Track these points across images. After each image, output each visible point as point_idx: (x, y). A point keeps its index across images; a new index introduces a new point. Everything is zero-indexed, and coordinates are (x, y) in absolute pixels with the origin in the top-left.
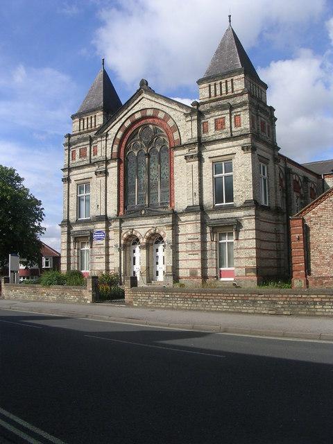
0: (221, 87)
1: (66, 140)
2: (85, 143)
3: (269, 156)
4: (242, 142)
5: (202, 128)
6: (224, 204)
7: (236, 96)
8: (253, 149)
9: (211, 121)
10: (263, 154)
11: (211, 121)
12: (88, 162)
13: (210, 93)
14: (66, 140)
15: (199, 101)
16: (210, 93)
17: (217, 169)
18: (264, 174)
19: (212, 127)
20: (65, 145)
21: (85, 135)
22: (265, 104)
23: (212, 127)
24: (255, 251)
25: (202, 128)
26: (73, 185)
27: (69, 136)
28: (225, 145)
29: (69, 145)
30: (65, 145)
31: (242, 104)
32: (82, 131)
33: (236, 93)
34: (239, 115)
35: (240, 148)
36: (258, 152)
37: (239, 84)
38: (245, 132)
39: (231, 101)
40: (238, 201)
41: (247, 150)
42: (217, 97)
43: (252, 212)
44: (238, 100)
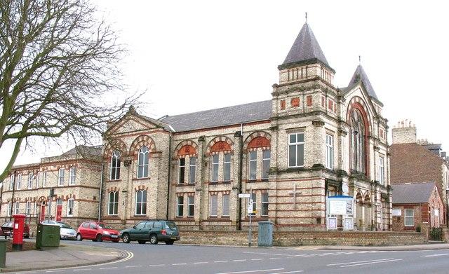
3: (335, 129)
7: (308, 81)
19: (288, 105)
21: (300, 85)
23: (288, 105)
35: (311, 123)
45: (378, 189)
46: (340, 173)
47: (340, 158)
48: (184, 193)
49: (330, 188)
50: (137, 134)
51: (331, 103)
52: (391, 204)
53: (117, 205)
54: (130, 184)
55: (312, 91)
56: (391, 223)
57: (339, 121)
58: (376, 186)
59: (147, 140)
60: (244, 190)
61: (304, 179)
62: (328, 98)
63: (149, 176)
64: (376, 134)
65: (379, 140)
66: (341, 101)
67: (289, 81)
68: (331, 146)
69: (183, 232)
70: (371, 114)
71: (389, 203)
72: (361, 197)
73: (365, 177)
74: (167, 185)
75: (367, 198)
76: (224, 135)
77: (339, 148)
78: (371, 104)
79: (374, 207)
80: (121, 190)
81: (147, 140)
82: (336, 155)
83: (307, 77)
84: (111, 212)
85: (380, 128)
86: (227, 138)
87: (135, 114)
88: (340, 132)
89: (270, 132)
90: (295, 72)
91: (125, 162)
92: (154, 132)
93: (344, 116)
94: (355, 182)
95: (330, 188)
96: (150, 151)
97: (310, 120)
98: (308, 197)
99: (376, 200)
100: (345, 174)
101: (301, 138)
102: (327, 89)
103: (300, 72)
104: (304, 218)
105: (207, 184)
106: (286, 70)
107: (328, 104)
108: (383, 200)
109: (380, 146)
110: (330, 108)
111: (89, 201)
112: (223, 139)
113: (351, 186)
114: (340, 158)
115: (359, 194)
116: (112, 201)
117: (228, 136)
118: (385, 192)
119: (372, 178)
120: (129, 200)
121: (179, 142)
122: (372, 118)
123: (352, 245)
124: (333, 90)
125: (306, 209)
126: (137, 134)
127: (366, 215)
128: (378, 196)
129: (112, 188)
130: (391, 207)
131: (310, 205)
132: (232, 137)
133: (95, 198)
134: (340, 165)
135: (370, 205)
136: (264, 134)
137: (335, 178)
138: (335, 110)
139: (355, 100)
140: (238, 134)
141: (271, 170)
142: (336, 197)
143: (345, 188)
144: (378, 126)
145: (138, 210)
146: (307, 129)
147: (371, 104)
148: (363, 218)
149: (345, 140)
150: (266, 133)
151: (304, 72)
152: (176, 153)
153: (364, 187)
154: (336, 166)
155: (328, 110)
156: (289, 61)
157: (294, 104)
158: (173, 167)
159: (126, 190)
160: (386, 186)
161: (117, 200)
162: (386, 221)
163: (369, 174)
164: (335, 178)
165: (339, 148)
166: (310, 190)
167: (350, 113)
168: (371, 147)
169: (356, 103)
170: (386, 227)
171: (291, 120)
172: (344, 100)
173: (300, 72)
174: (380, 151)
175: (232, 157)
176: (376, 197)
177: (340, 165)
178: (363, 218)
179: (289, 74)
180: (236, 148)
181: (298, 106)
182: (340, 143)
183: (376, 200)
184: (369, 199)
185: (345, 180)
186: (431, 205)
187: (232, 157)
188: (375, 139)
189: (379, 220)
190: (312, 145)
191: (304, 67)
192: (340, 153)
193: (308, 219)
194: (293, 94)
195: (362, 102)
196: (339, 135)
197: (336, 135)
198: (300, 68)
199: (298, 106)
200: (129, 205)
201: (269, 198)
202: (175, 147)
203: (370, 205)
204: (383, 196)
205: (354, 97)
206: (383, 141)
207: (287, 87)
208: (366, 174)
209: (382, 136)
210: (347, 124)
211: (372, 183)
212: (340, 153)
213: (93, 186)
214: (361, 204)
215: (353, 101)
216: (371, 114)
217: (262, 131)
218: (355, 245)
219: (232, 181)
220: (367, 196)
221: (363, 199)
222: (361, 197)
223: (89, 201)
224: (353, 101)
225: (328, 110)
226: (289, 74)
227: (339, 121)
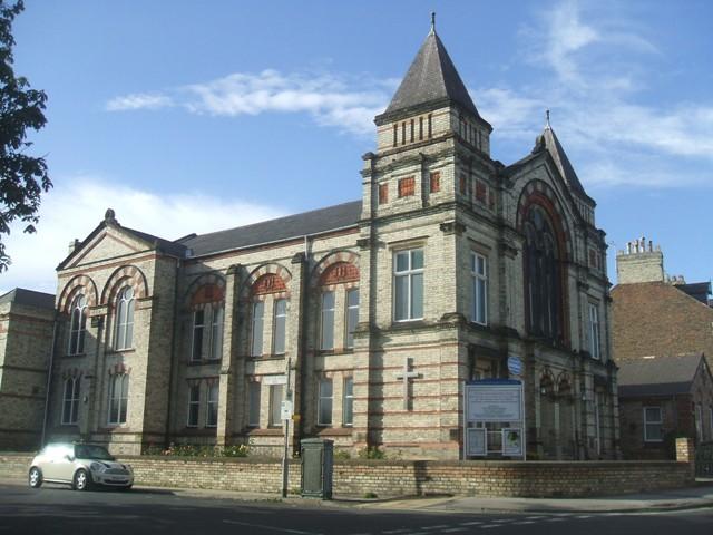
0: (417, 126)
1: (368, 165)
2: (414, 167)
3: (492, 243)
4: (441, 216)
5: (379, 195)
6: (409, 320)
7: (432, 142)
8: (457, 228)
9: (393, 186)
10: (477, 236)
11: (393, 186)
12: (419, 205)
13: (430, 123)
14: (368, 165)
15: (375, 153)
16: (430, 123)
17: (401, 263)
18: (481, 272)
19: (392, 193)
20: (364, 173)
21: (416, 152)
22: (486, 157)
23: (392, 193)
24: (366, 402)
25: (379, 195)
26: (385, 256)
27: (374, 158)
28: (405, 223)
29: (374, 173)
30: (364, 173)
31: (445, 154)
32: (399, 146)
33: (434, 137)
34: (413, 177)
35: (437, 227)
36: (470, 232)
37: (442, 120)
38: (446, 199)
39: (428, 150)
40: (431, 314)
41: (450, 229)
42: (416, 142)
43: (454, 333)
44: (437, 148)
45: (588, 367)
46: (504, 333)
47: (503, 303)
48: (200, 379)
49: (479, 364)
50: (113, 265)
51: (481, 189)
52: (615, 399)
53: (76, 404)
54: (101, 362)
55: (440, 163)
56: (617, 437)
57: (500, 225)
58: (582, 362)
59: (133, 272)
60: (405, 380)
61: (426, 345)
62: (474, 177)
63: (134, 346)
64: (580, 256)
65: (587, 269)
66: (504, 187)
67: (395, 145)
68: (484, 277)
69: (435, 428)
70: (570, 218)
71: (611, 395)
72: (551, 384)
73: (559, 342)
74: (169, 365)
75: (564, 385)
76: (274, 262)
77: (501, 282)
78: (570, 198)
79: (579, 405)
80: (85, 375)
81: (133, 272)
82: (494, 295)
83: (430, 135)
84: (67, 419)
85: (589, 247)
86: (280, 267)
87: (117, 226)
88: (503, 248)
89: (357, 250)
90: (408, 127)
91: (93, 318)
92: (143, 258)
93: (510, 215)
94: (536, 352)
95: (479, 364)
96: (138, 296)
97: (436, 222)
98: (433, 384)
99: (583, 389)
100: (514, 333)
101: (418, 261)
102: (472, 158)
103: (417, 127)
104: (426, 429)
105: (243, 361)
106: (391, 125)
107: (474, 188)
108: (599, 389)
109: (589, 282)
110: (480, 197)
111: (22, 397)
112: (273, 269)
113: (529, 363)
114: (503, 303)
115: (546, 377)
116: (69, 397)
117: (281, 262)
118: (604, 373)
119: (575, 346)
120: (98, 393)
121: (194, 278)
122: (571, 226)
123: (514, 496)
124: (485, 163)
125: (429, 409)
126: (113, 265)
127: (562, 420)
128: (588, 382)
129: (70, 370)
130: (616, 403)
131: (438, 401)
132: (287, 263)
133: (35, 390)
134: (503, 316)
135: (571, 400)
136: (348, 254)
137: (492, 343)
138: (492, 204)
139: (535, 188)
140: (302, 259)
141: (358, 328)
142: (493, 381)
143: (515, 365)
144: (586, 244)
145: (112, 413)
146: (429, 241)
147: (570, 198)
148: (557, 427)
149: (516, 265)
150: (354, 255)
151: (426, 126)
152: (188, 299)
153: (558, 365)
154: (493, 317)
155: (474, 201)
156: (400, 104)
157: (405, 190)
158: (183, 329)
159: (92, 374)
160: (604, 361)
161: (77, 395)
162: (607, 433)
163: (569, 335)
164: (492, 343)
165: (501, 282)
166: (437, 370)
167: (524, 211)
168: (571, 281)
169: (536, 191)
170: (607, 443)
171: (398, 224)
172: (510, 185)
173: (417, 127)
174: (591, 292)
175: (288, 304)
176: (583, 384)
177: (503, 316)
178: (557, 427)
179: (395, 133)
180: (294, 285)
181: (412, 193)
182: (502, 270)
183: (583, 389)
184: (568, 388)
185: (515, 347)
186: (695, 398)
187: (288, 304)
188: (578, 267)
189: (590, 432)
190: (440, 274)
191: (425, 116)
192: (502, 292)
193: (433, 432)
194: (402, 171)
195: (549, 193)
196: (501, 255)
197: (493, 254)
198: (417, 118)
199: (412, 193)
200: (97, 404)
201: (355, 388)
202: (186, 288)
203: (571, 400)
204: (597, 380)
205: (534, 182)
206: (595, 272)
207: (391, 157)
208: (562, 337)
209: (593, 263)
210: (519, 233)
211: (573, 354)
212: (502, 292)
213: (31, 366)
214: (552, 398)
215: (531, 190)
216: (570, 218)
217: (343, 250)
218: (519, 496)
219: (287, 353)
220: (564, 381)
221: (556, 388)
222: (551, 384)
223: (22, 397)
224: (531, 190)
225: (474, 201)
226: (395, 133)
227: (500, 225)
